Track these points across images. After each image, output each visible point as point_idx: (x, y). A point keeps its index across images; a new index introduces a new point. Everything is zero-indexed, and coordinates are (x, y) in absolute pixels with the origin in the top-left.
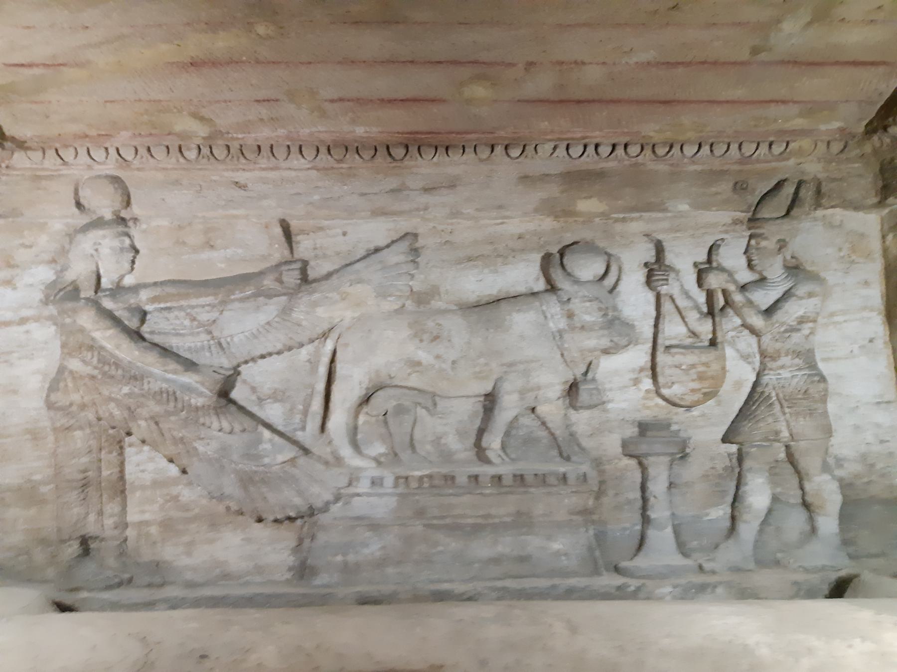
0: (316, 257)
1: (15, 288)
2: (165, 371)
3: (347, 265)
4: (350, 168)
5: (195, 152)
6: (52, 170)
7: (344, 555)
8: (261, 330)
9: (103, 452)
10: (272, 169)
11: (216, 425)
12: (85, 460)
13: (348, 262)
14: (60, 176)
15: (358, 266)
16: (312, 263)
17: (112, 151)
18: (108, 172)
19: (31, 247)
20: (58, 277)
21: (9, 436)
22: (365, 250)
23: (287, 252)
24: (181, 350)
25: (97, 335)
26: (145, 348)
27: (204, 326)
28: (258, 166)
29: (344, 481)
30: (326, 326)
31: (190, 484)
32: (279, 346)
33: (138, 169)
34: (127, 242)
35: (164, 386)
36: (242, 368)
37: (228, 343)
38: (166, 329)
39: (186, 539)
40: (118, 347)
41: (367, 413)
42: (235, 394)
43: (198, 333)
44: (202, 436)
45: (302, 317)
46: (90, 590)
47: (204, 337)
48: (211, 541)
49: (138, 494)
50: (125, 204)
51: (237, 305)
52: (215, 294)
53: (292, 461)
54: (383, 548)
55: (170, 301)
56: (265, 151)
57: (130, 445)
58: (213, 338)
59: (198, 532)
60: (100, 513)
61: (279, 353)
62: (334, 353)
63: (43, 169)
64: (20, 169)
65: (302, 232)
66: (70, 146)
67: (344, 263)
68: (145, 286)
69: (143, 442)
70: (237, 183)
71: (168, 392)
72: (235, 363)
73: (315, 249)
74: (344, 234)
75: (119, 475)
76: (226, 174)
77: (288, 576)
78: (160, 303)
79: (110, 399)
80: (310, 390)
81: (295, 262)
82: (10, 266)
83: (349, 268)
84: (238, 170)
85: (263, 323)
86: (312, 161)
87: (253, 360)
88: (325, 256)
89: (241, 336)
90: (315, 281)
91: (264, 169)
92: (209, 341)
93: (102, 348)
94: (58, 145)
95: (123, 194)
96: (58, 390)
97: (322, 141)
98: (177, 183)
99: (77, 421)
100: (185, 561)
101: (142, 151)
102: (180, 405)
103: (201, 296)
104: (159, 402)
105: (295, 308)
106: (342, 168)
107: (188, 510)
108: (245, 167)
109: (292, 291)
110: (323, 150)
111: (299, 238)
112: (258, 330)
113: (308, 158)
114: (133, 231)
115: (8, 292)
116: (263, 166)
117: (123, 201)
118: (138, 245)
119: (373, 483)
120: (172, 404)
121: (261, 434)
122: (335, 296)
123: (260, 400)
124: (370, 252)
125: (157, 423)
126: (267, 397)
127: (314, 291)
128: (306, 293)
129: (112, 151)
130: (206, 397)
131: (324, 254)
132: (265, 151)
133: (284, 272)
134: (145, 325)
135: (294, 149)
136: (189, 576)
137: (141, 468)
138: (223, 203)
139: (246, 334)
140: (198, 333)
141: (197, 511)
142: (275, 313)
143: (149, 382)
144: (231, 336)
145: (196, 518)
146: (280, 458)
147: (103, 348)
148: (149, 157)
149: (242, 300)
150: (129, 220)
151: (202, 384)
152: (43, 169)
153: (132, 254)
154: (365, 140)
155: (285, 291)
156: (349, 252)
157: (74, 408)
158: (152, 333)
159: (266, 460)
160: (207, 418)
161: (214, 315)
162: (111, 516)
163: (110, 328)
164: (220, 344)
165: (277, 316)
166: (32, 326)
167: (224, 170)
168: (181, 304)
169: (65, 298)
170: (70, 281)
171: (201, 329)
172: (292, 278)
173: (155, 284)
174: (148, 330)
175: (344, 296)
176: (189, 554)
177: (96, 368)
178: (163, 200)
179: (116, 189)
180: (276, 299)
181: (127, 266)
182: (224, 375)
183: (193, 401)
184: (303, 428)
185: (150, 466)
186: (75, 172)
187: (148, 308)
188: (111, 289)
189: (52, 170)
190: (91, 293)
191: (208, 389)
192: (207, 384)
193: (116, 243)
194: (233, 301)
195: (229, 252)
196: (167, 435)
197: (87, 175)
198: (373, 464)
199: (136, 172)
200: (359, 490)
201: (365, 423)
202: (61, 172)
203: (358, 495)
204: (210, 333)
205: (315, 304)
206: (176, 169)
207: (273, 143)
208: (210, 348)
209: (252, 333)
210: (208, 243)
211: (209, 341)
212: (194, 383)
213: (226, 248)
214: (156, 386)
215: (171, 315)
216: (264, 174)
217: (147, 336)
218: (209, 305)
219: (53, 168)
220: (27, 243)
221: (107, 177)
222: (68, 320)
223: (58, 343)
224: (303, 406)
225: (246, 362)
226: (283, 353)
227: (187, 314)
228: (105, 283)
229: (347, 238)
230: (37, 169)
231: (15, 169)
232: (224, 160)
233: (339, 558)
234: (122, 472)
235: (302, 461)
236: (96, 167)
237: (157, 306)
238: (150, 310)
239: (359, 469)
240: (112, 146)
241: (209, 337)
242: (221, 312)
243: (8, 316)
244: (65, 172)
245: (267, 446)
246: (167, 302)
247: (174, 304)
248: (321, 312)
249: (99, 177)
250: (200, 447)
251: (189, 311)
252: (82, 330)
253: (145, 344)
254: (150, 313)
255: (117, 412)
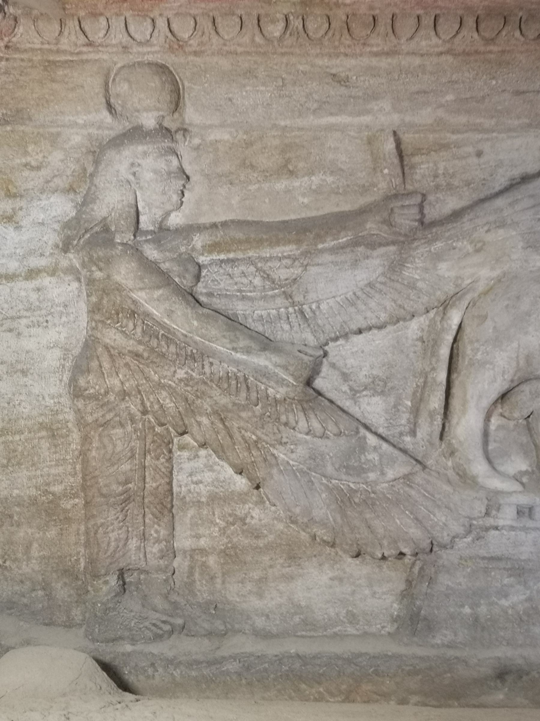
0: (437, 187)
1: (18, 228)
2: (234, 349)
3: (482, 201)
4: (503, 52)
5: (281, 25)
6: (72, 54)
7: (474, 606)
8: (359, 293)
9: (148, 458)
10: (387, 54)
11: (303, 424)
12: (126, 467)
13: (482, 196)
14: (83, 62)
15: (500, 202)
16: (431, 198)
17: (161, 23)
18: (150, 58)
19: (38, 168)
20: (79, 212)
21: (21, 432)
22: (507, 179)
23: (399, 180)
24: (250, 320)
25: (140, 296)
26: (208, 316)
27: (281, 286)
28: (368, 49)
29: (480, 508)
30: (450, 289)
31: (260, 502)
32: (383, 317)
33: (195, 53)
34: (175, 162)
35: (233, 369)
36: (331, 347)
37: (313, 312)
38: (227, 290)
39: (256, 575)
40: (170, 314)
41: (502, 415)
42: (319, 383)
43: (273, 297)
44: (284, 440)
45: (417, 277)
46: (133, 641)
47: (280, 301)
48: (289, 578)
49: (191, 512)
50: (173, 106)
51: (327, 258)
52: (298, 242)
53: (407, 478)
54: (530, 599)
55: (235, 251)
56: (383, 26)
57: (182, 448)
58: (293, 304)
59: (271, 567)
60: (144, 537)
61: (380, 327)
62: (460, 327)
63: (58, 51)
64: (25, 51)
65: (418, 151)
66: (101, 14)
67: (475, 196)
68: (200, 228)
69: (203, 445)
70: (334, 75)
71: (237, 378)
72: (322, 339)
73: (436, 176)
74: (479, 154)
75: (167, 487)
76: (319, 62)
77: (390, 628)
78: (219, 252)
79: (161, 386)
80: (422, 380)
81: (410, 194)
82: (10, 195)
83: (487, 205)
84: (337, 56)
85: (362, 284)
86: (448, 41)
87: (346, 336)
88: (450, 187)
89: (331, 302)
90: (433, 224)
91: (376, 54)
92: (287, 308)
93: (148, 315)
94: (82, 13)
95: (171, 91)
96: (89, 371)
97: (469, 9)
98: (250, 73)
99: (116, 415)
100: (255, 603)
101: (206, 24)
102: (254, 395)
103: (278, 243)
104: (227, 391)
105: (408, 263)
106: (490, 52)
107: (257, 537)
108: (348, 51)
109: (402, 239)
110: (470, 22)
111: (417, 159)
112: (354, 294)
113: (443, 37)
114: (183, 148)
115: (10, 232)
116: (375, 49)
117: (171, 102)
118: (188, 169)
119: (520, 513)
120: (243, 394)
121: (365, 438)
122: (466, 246)
123: (354, 394)
124: (514, 182)
125: (222, 421)
126: (362, 389)
127: (435, 239)
128: (423, 241)
129: (161, 23)
130: (288, 386)
131: (448, 184)
132: (383, 26)
133: (396, 210)
134: (200, 284)
135: (428, 21)
136: (260, 622)
137: (195, 479)
138: (315, 105)
139: (338, 299)
140: (273, 297)
141: (271, 538)
142: (380, 270)
143: (211, 364)
144: (318, 302)
145: (269, 547)
146: (391, 474)
147: (148, 315)
148: (213, 32)
149: (333, 250)
150: (176, 132)
151: (285, 368)
152: (58, 51)
153: (183, 182)
154: (533, 6)
155: (391, 238)
156: (484, 182)
157: (112, 397)
158: (210, 295)
159: (372, 476)
160: (291, 416)
161: (297, 271)
162: (158, 541)
163: (159, 287)
164: (302, 312)
165: (383, 274)
166: (46, 281)
167: (317, 55)
168: (248, 255)
169: (92, 244)
170: (100, 219)
171: (277, 291)
172: (408, 219)
173: (214, 226)
174: (204, 291)
175: (479, 245)
176: (260, 595)
177: (140, 342)
178: (230, 100)
179: (163, 83)
180: (382, 250)
181: (175, 198)
182: (311, 356)
183: (271, 391)
184: (413, 433)
185: (208, 476)
186: (105, 57)
187: (202, 259)
188: (152, 232)
189: (72, 54)
190: (128, 237)
191: (292, 375)
192: (291, 368)
193: (161, 165)
194: (322, 251)
195: (316, 180)
196: (237, 436)
197: (121, 61)
198: (517, 487)
199: (191, 58)
200: (501, 523)
201: (500, 427)
202: (85, 57)
203: (496, 528)
204: (288, 296)
205: (438, 257)
206: (248, 53)
207: (397, 11)
208: (288, 318)
209: (347, 298)
210: (286, 166)
211: (287, 308)
212: (270, 367)
213: (311, 173)
214: (220, 369)
215: (236, 271)
216: (374, 61)
217: (203, 299)
218: (289, 257)
219: (72, 49)
220: (33, 163)
221: (150, 64)
222: (98, 275)
223: (83, 307)
224: (411, 402)
225: (336, 339)
226: (386, 326)
227: (258, 270)
228: (145, 222)
229: (482, 160)
230: (50, 51)
231: (17, 50)
232: (320, 39)
233: (467, 610)
234: (170, 484)
235: (420, 478)
236: (135, 49)
237: (215, 257)
238: (206, 263)
239: (498, 493)
240: (161, 15)
241: (287, 303)
242: (305, 267)
243: (13, 266)
244: (92, 56)
245: (373, 456)
246: (229, 251)
247: (240, 255)
248: (443, 267)
249: (140, 64)
250: (281, 454)
251: (259, 265)
252: (119, 288)
253: (201, 310)
254: (205, 266)
255: (169, 404)
